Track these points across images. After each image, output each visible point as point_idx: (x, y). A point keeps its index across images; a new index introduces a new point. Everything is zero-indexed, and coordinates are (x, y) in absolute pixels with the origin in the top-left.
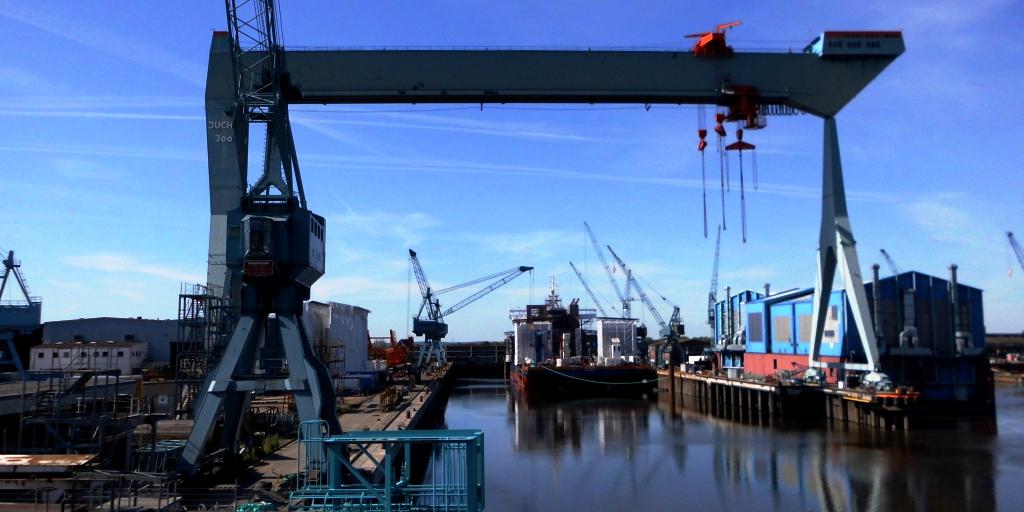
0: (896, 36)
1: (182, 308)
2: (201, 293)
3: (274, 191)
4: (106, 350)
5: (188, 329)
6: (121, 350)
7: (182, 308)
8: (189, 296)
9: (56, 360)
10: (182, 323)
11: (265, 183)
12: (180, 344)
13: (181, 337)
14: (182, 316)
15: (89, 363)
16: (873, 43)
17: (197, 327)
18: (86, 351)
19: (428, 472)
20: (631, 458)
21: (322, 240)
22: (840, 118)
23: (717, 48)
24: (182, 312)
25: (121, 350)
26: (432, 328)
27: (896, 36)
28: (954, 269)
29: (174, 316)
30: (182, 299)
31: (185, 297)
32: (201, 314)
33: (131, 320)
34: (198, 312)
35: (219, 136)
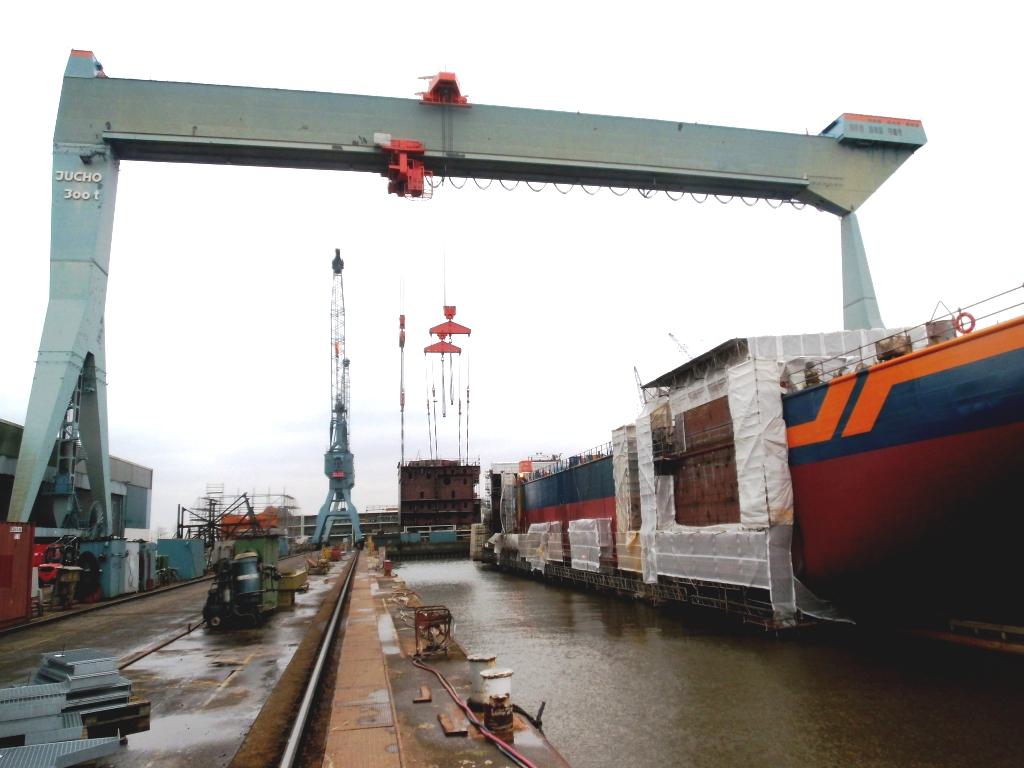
22: (863, 214)
23: (445, 91)
35: (70, 191)
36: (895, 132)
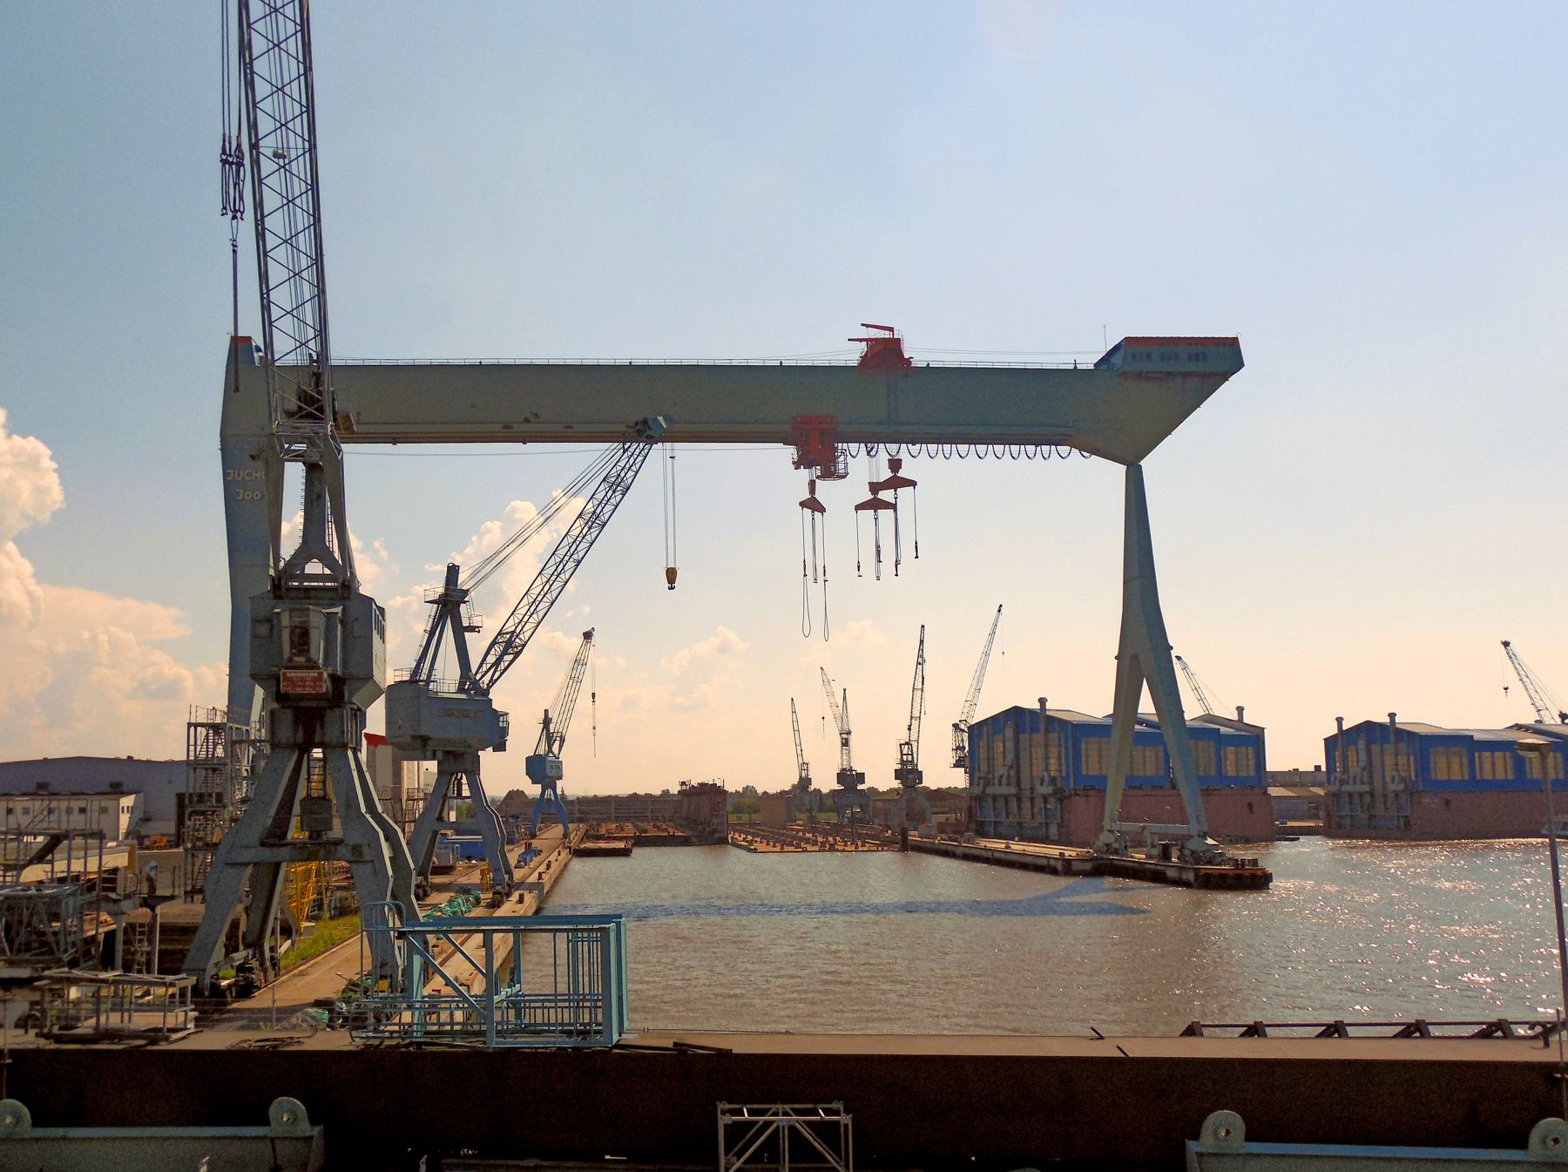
0: (1232, 344)
1: (192, 742)
2: (218, 720)
3: (314, 568)
4: (82, 804)
5: (201, 773)
6: (104, 804)
7: (192, 742)
8: (202, 725)
9: (11, 818)
10: (192, 765)
11: (303, 555)
12: (191, 795)
13: (191, 785)
14: (192, 753)
15: (59, 821)
16: (1197, 355)
17: (214, 770)
18: (54, 804)
19: (187, 925)
20: (101, 842)
21: (384, 642)
22: (1150, 465)
24: (192, 748)
25: (104, 804)
26: (805, 782)
27: (1232, 344)
28: (1240, 710)
29: (180, 755)
30: (192, 729)
31: (196, 725)
32: (220, 752)
33: (117, 760)
34: (214, 749)
36: (1195, 357)
